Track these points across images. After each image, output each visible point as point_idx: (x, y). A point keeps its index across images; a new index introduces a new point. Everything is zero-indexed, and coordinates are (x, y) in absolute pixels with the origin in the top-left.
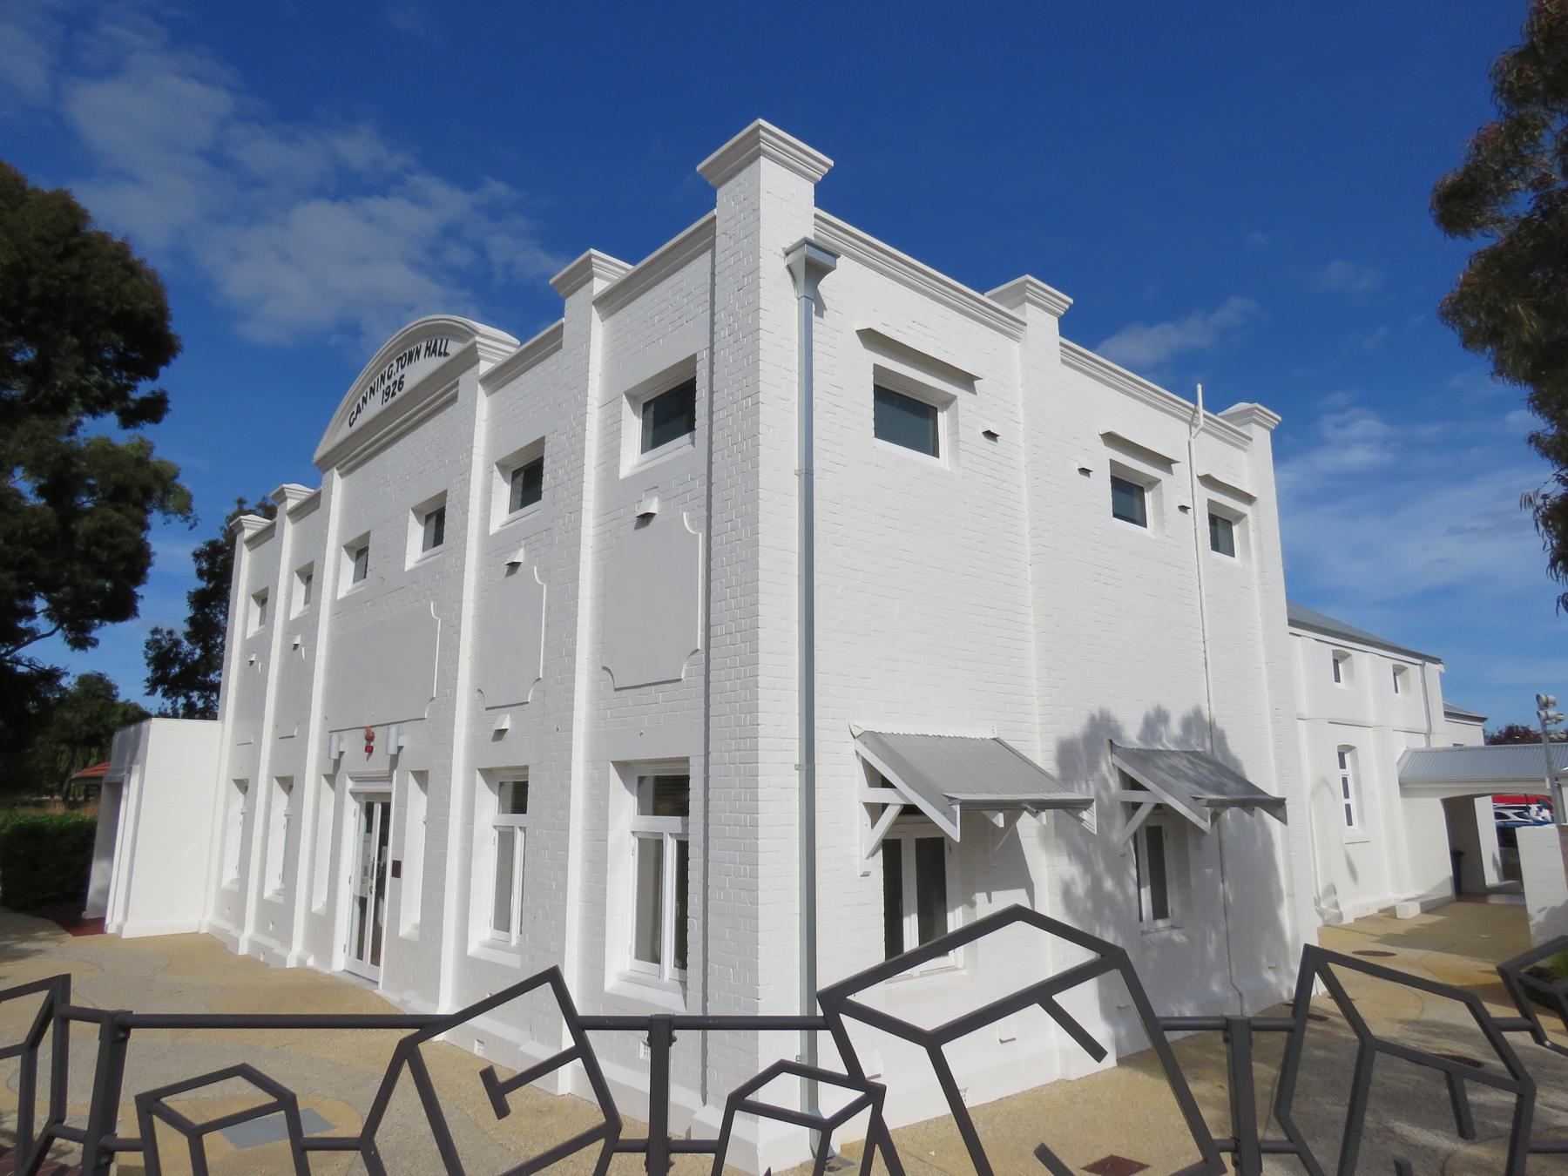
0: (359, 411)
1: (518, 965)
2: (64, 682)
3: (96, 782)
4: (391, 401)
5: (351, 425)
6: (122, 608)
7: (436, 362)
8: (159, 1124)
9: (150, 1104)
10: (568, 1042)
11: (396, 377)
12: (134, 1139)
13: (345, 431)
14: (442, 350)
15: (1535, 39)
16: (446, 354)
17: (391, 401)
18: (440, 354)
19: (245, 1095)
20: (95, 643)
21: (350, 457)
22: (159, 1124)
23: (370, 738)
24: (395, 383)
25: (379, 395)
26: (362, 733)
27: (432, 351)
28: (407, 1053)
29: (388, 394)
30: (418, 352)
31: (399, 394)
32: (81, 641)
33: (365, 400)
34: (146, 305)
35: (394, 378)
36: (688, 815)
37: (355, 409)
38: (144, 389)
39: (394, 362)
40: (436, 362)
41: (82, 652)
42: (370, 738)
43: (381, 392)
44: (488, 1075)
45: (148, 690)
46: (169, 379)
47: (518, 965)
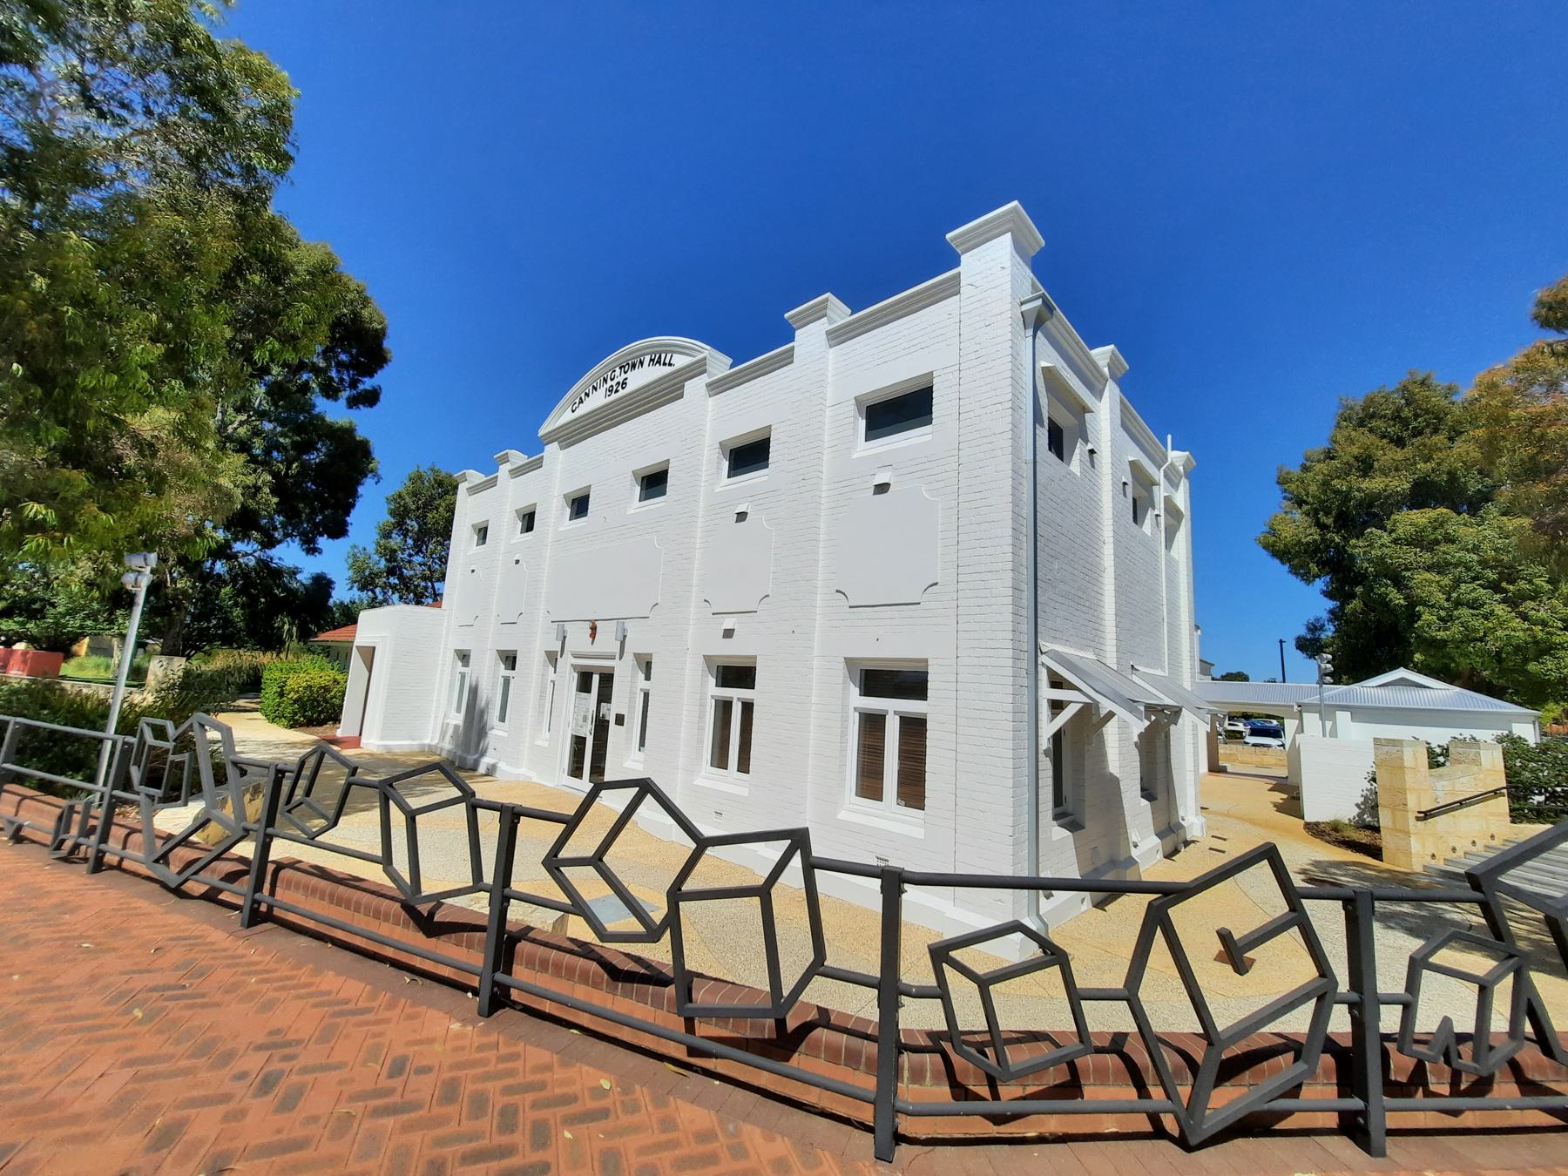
0: (581, 401)
1: (642, 769)
2: (299, 577)
3: (347, 645)
4: (614, 396)
5: (573, 411)
6: (338, 530)
7: (660, 371)
8: (949, 971)
9: (941, 954)
10: (1281, 907)
11: (621, 379)
12: (931, 987)
13: (568, 416)
14: (667, 361)
15: (343, 357)
16: (670, 365)
17: (614, 396)
18: (665, 364)
19: (1015, 949)
20: (319, 551)
21: (571, 436)
22: (949, 971)
23: (594, 629)
24: (618, 383)
25: (602, 391)
26: (588, 625)
27: (657, 361)
28: (1156, 920)
29: (611, 391)
30: (641, 363)
31: (622, 393)
32: (311, 549)
33: (587, 395)
34: (376, 325)
35: (616, 381)
36: (1062, 701)
37: (577, 401)
38: (367, 384)
39: (617, 369)
40: (660, 371)
41: (313, 557)
42: (594, 629)
43: (603, 389)
44: (1224, 936)
45: (349, 586)
46: (380, 379)
47: (642, 769)
